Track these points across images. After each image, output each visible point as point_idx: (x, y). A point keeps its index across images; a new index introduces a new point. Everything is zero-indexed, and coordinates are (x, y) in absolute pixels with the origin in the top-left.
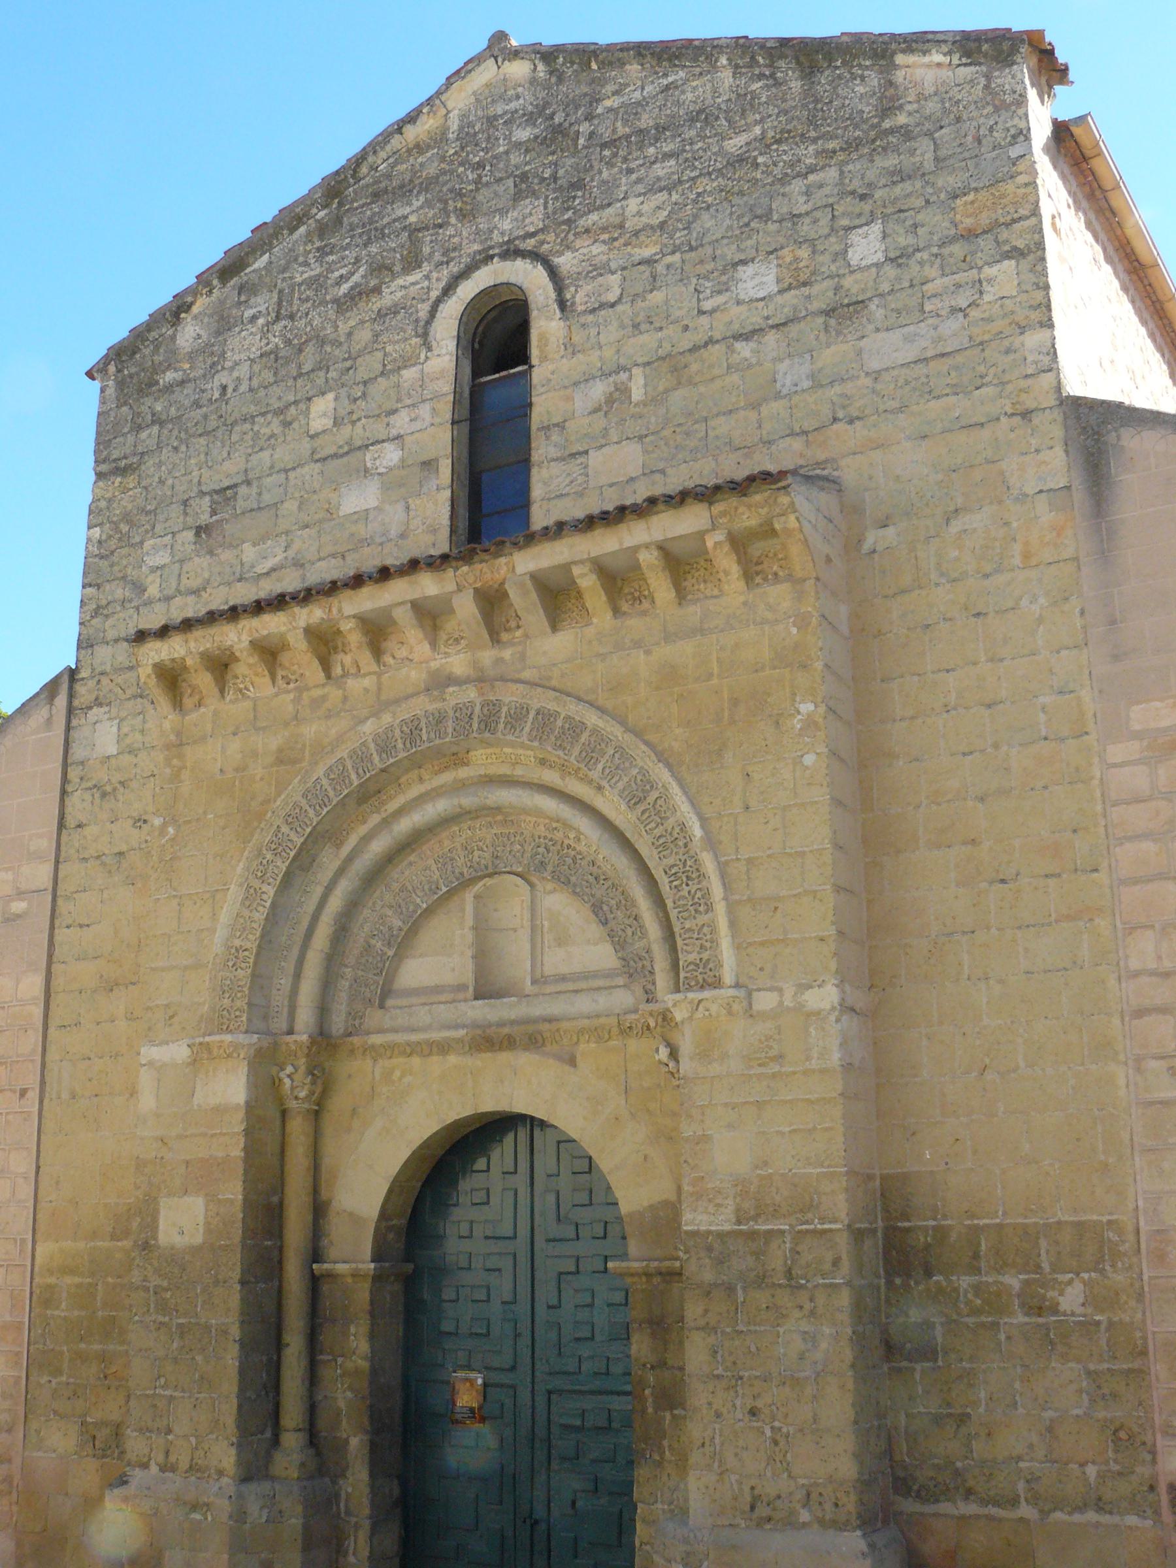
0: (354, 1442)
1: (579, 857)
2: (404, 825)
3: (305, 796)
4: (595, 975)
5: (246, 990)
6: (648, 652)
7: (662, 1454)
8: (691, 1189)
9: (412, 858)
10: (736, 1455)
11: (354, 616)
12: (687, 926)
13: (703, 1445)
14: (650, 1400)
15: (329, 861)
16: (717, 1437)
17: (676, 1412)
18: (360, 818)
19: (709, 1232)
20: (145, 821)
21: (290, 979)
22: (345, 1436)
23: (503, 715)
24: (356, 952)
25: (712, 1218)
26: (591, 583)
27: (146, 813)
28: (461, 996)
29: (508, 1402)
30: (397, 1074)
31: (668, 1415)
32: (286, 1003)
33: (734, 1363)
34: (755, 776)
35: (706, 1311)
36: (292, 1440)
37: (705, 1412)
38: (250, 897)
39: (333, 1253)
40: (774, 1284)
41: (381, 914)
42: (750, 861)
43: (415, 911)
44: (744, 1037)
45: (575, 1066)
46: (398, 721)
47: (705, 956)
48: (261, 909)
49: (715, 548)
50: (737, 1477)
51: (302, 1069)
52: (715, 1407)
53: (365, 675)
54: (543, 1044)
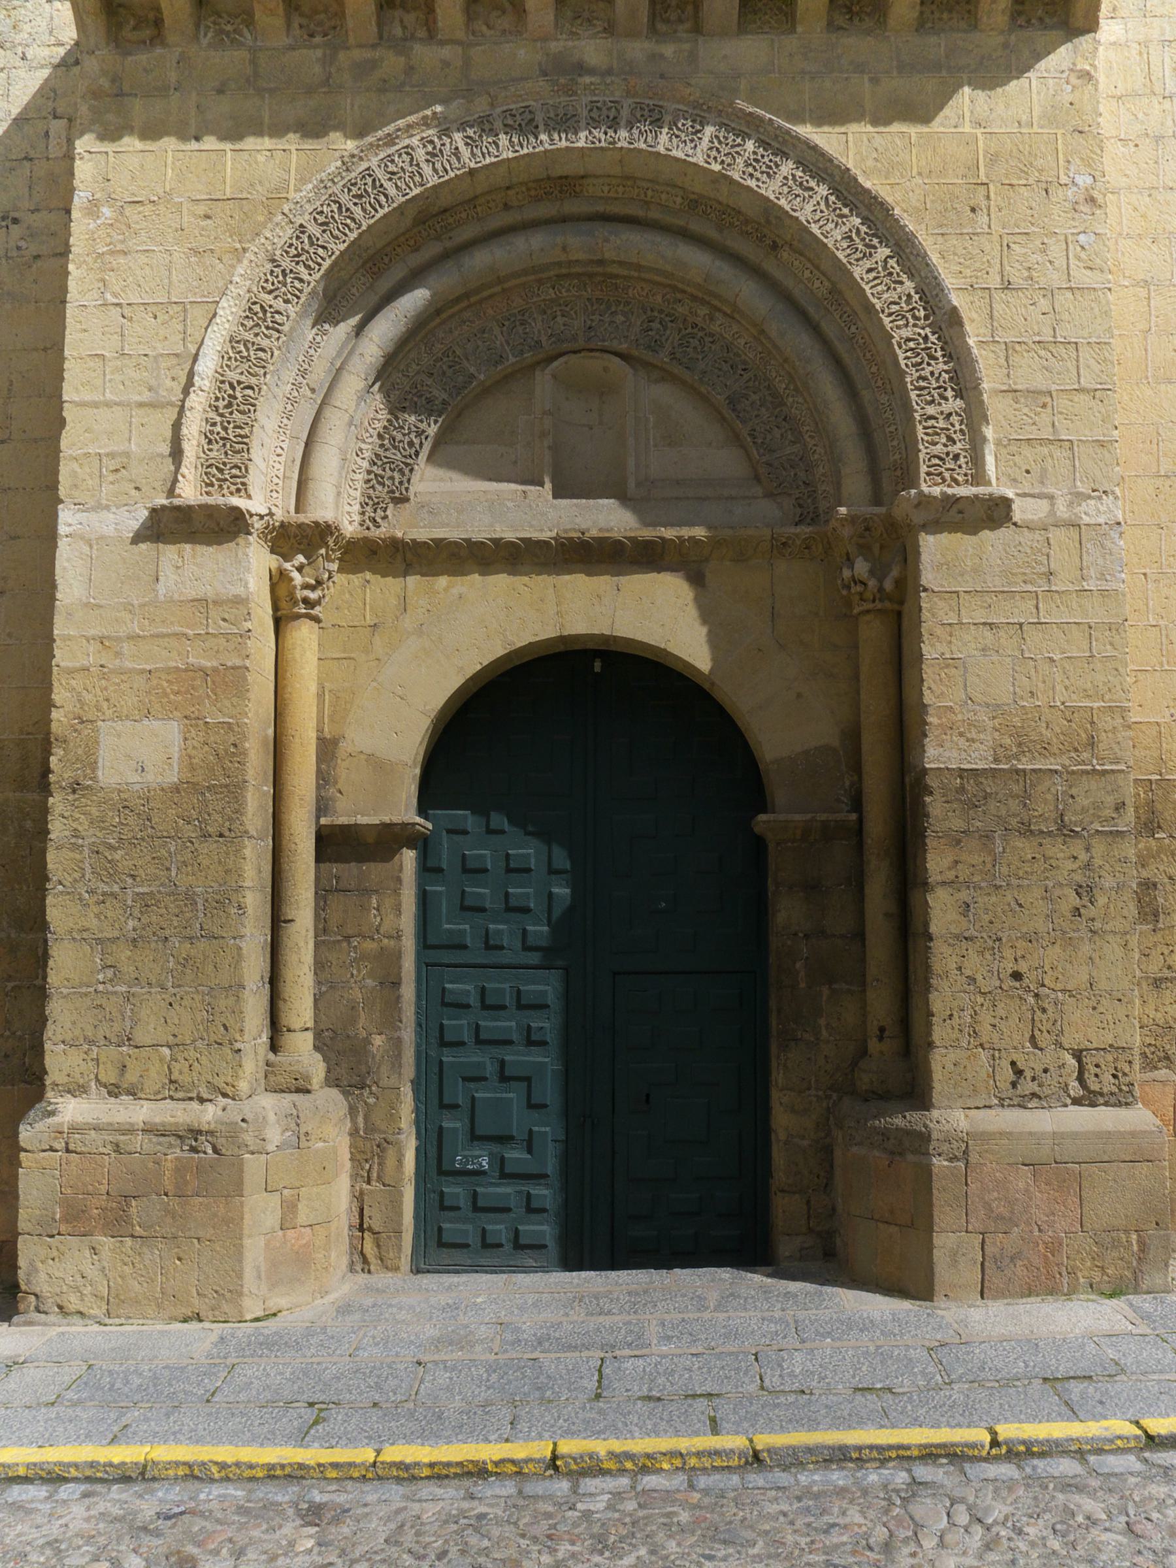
1: (708, 339)
6: (875, 81)
13: (951, 1016)
14: (802, 974)
17: (835, 986)
20: (15, 221)
25: (964, 755)
27: (16, 209)
31: (826, 991)
40: (1042, 832)
46: (499, 110)
53: (442, 43)
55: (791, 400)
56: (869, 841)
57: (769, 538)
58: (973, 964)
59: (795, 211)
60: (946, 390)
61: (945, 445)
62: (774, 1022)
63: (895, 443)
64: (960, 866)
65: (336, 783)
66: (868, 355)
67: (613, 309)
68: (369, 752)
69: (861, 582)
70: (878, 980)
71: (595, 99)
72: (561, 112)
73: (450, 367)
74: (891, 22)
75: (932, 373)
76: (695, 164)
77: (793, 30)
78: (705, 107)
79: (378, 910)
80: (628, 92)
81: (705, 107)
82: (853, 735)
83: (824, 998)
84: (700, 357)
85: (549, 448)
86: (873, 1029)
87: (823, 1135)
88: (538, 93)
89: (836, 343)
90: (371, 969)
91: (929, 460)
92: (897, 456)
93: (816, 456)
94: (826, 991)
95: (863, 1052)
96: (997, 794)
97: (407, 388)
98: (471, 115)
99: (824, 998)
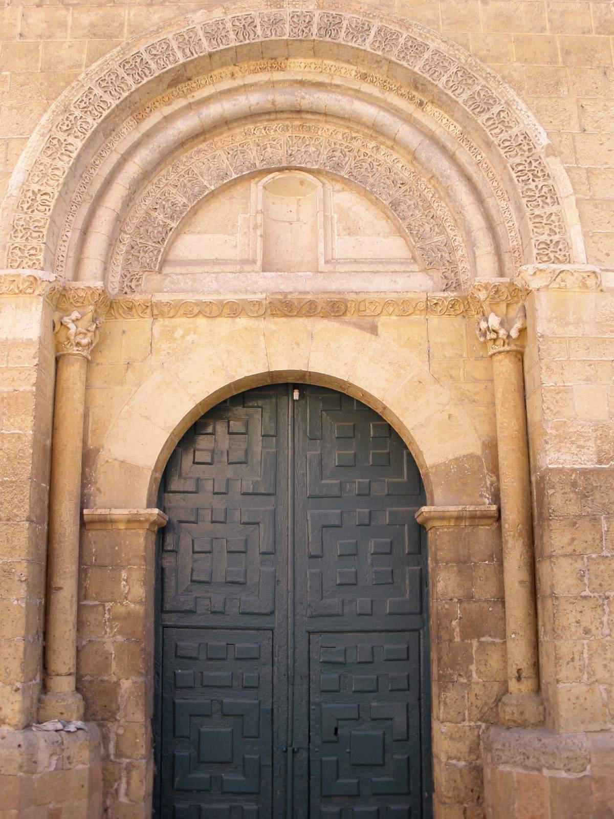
0: (126, 684)
2: (214, 111)
3: (123, 65)
4: (388, 262)
7: (469, 677)
8: (554, 432)
9: (203, 146)
10: (605, 666)
12: (536, 213)
13: (573, 659)
14: (458, 629)
15: (129, 134)
16: (586, 651)
17: (483, 639)
19: (574, 470)
22: (115, 679)
23: (344, 26)
24: (135, 221)
25: (575, 458)
28: (248, 268)
29: (266, 643)
31: (475, 643)
32: (71, 254)
33: (601, 585)
34: (588, 108)
35: (573, 539)
36: (63, 685)
37: (573, 629)
38: (52, 146)
39: (100, 499)
41: (170, 186)
42: (588, 170)
43: (201, 192)
44: (596, 307)
46: (230, 17)
47: (556, 238)
48: (66, 158)
50: (605, 686)
51: (89, 316)
52: (584, 624)
54: (344, 314)
55: (436, 205)
56: (507, 526)
57: (425, 300)
58: (588, 618)
59: (435, 80)
60: (547, 198)
61: (549, 235)
62: (435, 669)
63: (513, 234)
64: (576, 543)
65: (96, 483)
66: (490, 175)
67: (307, 143)
68: (121, 459)
69: (494, 331)
70: (515, 633)
71: (296, 10)
72: (272, 18)
73: (190, 181)
75: (536, 186)
76: (365, 50)
78: (371, 16)
79: (126, 582)
80: (318, 6)
81: (371, 16)
82: (492, 447)
83: (474, 649)
85: (261, 236)
86: (512, 672)
87: (475, 757)
88: (257, 6)
89: (468, 166)
90: (121, 627)
91: (539, 245)
92: (515, 243)
93: (456, 243)
94: (475, 643)
95: (506, 691)
96: (601, 487)
97: (158, 196)
98: (211, 20)
99: (474, 649)
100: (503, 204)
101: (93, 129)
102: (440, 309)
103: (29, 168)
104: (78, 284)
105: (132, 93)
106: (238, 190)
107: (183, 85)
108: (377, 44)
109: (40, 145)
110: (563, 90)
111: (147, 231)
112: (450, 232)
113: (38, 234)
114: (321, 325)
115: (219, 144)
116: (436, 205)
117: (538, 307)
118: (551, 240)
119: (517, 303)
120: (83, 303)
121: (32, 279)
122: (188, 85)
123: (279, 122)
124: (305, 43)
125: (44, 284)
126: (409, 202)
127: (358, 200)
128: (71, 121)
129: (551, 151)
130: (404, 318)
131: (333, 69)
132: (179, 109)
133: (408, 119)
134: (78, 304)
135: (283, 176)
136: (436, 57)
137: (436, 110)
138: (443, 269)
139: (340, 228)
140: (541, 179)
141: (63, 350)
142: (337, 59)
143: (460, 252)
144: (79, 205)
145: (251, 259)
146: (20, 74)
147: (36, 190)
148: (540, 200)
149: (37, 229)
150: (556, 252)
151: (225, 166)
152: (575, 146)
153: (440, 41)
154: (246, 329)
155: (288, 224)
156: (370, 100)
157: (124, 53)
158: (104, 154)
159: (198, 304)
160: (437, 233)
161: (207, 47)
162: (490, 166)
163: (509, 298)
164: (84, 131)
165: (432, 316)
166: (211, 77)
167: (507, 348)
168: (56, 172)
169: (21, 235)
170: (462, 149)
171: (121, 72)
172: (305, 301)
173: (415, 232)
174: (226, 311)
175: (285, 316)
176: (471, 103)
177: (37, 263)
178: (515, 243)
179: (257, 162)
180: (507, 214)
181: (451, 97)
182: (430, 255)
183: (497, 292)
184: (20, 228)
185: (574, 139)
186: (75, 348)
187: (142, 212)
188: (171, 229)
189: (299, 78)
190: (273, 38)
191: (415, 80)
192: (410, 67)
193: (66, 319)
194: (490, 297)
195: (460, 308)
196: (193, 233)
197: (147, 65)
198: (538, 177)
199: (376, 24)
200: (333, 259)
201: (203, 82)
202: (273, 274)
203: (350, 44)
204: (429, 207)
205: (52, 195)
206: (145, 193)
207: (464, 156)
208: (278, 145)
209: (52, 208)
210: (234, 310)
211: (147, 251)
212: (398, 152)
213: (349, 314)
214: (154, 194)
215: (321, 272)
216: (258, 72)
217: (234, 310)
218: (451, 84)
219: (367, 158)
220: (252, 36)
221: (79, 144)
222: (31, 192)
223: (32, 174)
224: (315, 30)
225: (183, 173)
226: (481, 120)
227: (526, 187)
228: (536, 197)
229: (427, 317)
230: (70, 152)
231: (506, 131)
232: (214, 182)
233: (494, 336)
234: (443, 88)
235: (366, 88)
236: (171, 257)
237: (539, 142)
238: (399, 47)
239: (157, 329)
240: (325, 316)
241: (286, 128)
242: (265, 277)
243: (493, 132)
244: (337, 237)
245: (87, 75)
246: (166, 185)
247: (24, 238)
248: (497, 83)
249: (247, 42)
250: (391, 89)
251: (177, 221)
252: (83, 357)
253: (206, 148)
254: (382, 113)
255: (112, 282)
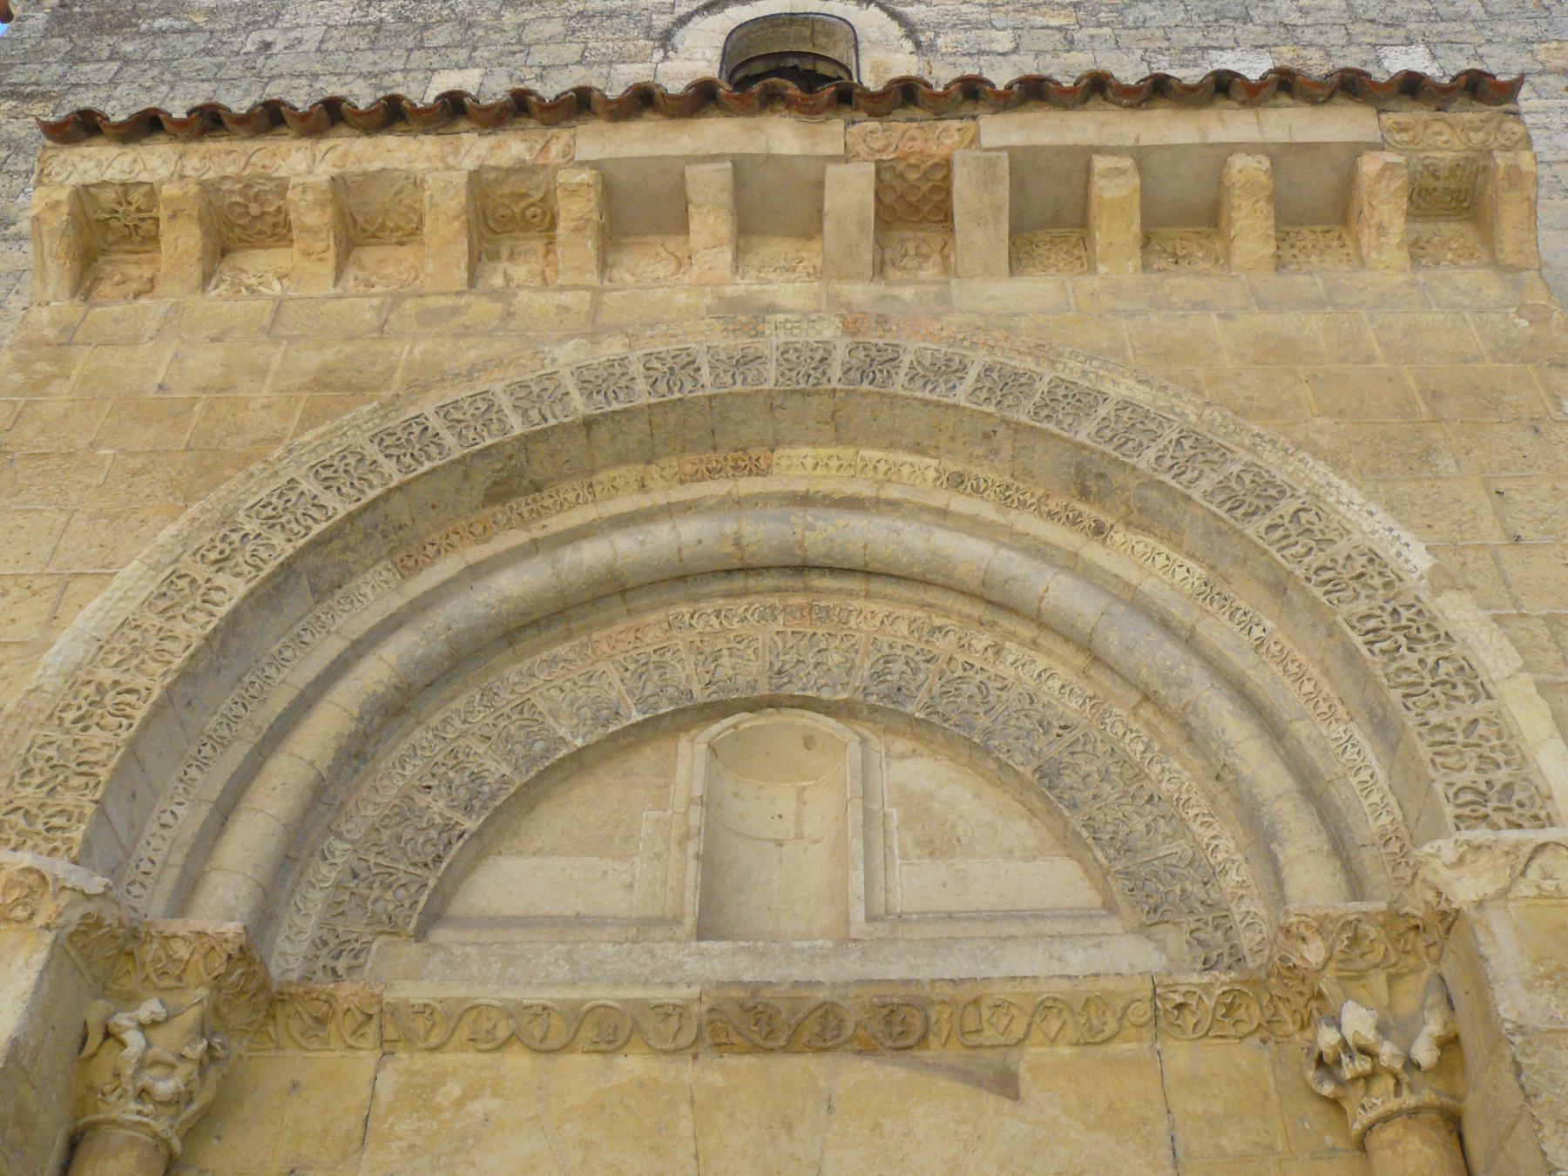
2: (592, 555)
5: (104, 774)
9: (562, 650)
11: (595, 165)
15: (375, 594)
18: (478, 529)
21: (204, 811)
26: (1125, 192)
30: (454, 1089)
32: (178, 859)
38: (171, 592)
41: (471, 735)
45: (1016, 1097)
46: (639, 353)
47: (1501, 776)
49: (1380, 176)
51: (191, 1016)
54: (923, 1041)
55: (1157, 768)
57: (1150, 994)
59: (1130, 457)
60: (1454, 686)
63: (1375, 798)
66: (1293, 668)
67: (822, 646)
69: (1363, 1051)
73: (521, 728)
74: (1237, 260)
77: (1092, 269)
81: (966, 343)
84: (981, 710)
85: (697, 856)
88: (703, 333)
91: (1456, 795)
92: (1385, 819)
93: (1220, 856)
97: (439, 758)
100: (1337, 730)
101: (281, 559)
102: (1192, 1021)
103: (104, 635)
104: (178, 926)
105: (390, 491)
106: (646, 759)
107: (522, 499)
108: (983, 395)
109: (143, 588)
110: (1446, 464)
111: (399, 838)
112: (1201, 830)
113: (85, 779)
114: (853, 1074)
115: (604, 647)
116: (1157, 768)
117: (1487, 950)
118: (1488, 783)
119: (1415, 971)
120: (179, 979)
121: (32, 879)
122: (534, 500)
123: (752, 598)
124: (814, 401)
125: (65, 898)
126: (1086, 769)
127: (953, 775)
128: (231, 543)
129: (1442, 580)
130: (1091, 1049)
131: (882, 467)
132: (508, 551)
133: (1072, 564)
134: (165, 983)
135: (761, 721)
136: (1125, 415)
137: (1135, 538)
138: (1189, 922)
139: (908, 840)
140: (1431, 644)
141: (97, 1111)
142: (892, 446)
143: (1233, 875)
144: (224, 744)
145: (668, 915)
146: (134, 455)
147: (108, 683)
148: (1436, 691)
149: (84, 768)
150: (1509, 809)
151: (614, 694)
152: (1502, 574)
153: (1132, 382)
154: (641, 1085)
155: (772, 845)
156: (975, 526)
157: (386, 415)
158: (307, 638)
159: (510, 1011)
160: (1166, 836)
161: (580, 406)
162: (1288, 645)
163: (1393, 959)
164: (259, 562)
165: (1171, 1043)
166: (591, 485)
167: (1409, 1100)
168: (168, 645)
169: (37, 780)
170: (1211, 620)
171: (372, 451)
172: (811, 1004)
173: (1107, 837)
174: (588, 1033)
175: (755, 1049)
176: (1222, 497)
177: (63, 848)
178: (1385, 819)
179: (696, 688)
180: (1351, 753)
181: (1171, 488)
182: (1146, 892)
183: (1355, 940)
184: (41, 764)
185: (1497, 560)
186: (132, 1106)
187: (393, 792)
188: (461, 836)
189: (801, 487)
190: (738, 388)
191: (1079, 468)
192: (1065, 434)
193: (122, 1019)
194: (1337, 955)
195: (1252, 1014)
196: (520, 853)
197: (436, 440)
198: (1423, 641)
199: (981, 358)
200: (888, 913)
201: (571, 496)
202: (724, 945)
203: (919, 394)
204: (1139, 776)
205: (144, 692)
206: (404, 746)
207: (1218, 633)
208: (750, 651)
209: (136, 722)
210: (611, 1031)
211: (391, 886)
212: (1049, 653)
213: (934, 1042)
214: (428, 754)
215: (855, 940)
216: (704, 479)
217: (611, 1031)
218: (1168, 462)
219: (971, 673)
220: (689, 385)
221: (241, 588)
222: (93, 686)
223: (107, 647)
224: (836, 372)
225: (507, 710)
226: (1253, 529)
227: (1394, 666)
228: (1427, 686)
229: (1158, 1046)
230: (215, 604)
231: (1321, 550)
232: (583, 730)
233: (1363, 1065)
234: (1149, 472)
235: (961, 504)
236: (458, 907)
237: (1409, 567)
238: (1037, 398)
239: (388, 1082)
240: (867, 1049)
241: (770, 614)
242: (702, 954)
243: (1286, 552)
244: (898, 862)
245: (290, 451)
246: (463, 735)
247: (45, 789)
248: (1281, 453)
249: (677, 395)
250: (1023, 504)
251: (479, 816)
252: (155, 1135)
253: (571, 655)
254: (1003, 553)
255: (283, 954)
